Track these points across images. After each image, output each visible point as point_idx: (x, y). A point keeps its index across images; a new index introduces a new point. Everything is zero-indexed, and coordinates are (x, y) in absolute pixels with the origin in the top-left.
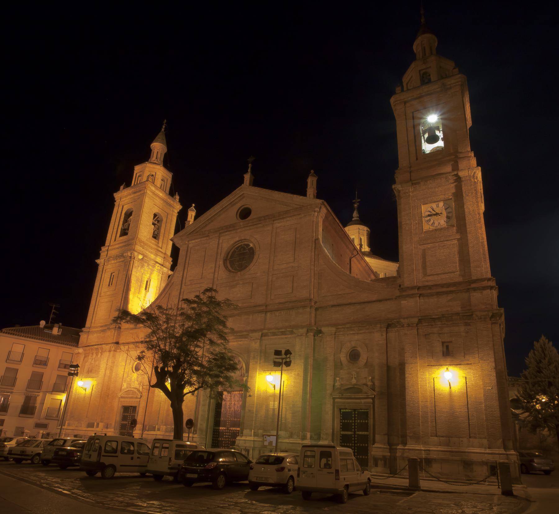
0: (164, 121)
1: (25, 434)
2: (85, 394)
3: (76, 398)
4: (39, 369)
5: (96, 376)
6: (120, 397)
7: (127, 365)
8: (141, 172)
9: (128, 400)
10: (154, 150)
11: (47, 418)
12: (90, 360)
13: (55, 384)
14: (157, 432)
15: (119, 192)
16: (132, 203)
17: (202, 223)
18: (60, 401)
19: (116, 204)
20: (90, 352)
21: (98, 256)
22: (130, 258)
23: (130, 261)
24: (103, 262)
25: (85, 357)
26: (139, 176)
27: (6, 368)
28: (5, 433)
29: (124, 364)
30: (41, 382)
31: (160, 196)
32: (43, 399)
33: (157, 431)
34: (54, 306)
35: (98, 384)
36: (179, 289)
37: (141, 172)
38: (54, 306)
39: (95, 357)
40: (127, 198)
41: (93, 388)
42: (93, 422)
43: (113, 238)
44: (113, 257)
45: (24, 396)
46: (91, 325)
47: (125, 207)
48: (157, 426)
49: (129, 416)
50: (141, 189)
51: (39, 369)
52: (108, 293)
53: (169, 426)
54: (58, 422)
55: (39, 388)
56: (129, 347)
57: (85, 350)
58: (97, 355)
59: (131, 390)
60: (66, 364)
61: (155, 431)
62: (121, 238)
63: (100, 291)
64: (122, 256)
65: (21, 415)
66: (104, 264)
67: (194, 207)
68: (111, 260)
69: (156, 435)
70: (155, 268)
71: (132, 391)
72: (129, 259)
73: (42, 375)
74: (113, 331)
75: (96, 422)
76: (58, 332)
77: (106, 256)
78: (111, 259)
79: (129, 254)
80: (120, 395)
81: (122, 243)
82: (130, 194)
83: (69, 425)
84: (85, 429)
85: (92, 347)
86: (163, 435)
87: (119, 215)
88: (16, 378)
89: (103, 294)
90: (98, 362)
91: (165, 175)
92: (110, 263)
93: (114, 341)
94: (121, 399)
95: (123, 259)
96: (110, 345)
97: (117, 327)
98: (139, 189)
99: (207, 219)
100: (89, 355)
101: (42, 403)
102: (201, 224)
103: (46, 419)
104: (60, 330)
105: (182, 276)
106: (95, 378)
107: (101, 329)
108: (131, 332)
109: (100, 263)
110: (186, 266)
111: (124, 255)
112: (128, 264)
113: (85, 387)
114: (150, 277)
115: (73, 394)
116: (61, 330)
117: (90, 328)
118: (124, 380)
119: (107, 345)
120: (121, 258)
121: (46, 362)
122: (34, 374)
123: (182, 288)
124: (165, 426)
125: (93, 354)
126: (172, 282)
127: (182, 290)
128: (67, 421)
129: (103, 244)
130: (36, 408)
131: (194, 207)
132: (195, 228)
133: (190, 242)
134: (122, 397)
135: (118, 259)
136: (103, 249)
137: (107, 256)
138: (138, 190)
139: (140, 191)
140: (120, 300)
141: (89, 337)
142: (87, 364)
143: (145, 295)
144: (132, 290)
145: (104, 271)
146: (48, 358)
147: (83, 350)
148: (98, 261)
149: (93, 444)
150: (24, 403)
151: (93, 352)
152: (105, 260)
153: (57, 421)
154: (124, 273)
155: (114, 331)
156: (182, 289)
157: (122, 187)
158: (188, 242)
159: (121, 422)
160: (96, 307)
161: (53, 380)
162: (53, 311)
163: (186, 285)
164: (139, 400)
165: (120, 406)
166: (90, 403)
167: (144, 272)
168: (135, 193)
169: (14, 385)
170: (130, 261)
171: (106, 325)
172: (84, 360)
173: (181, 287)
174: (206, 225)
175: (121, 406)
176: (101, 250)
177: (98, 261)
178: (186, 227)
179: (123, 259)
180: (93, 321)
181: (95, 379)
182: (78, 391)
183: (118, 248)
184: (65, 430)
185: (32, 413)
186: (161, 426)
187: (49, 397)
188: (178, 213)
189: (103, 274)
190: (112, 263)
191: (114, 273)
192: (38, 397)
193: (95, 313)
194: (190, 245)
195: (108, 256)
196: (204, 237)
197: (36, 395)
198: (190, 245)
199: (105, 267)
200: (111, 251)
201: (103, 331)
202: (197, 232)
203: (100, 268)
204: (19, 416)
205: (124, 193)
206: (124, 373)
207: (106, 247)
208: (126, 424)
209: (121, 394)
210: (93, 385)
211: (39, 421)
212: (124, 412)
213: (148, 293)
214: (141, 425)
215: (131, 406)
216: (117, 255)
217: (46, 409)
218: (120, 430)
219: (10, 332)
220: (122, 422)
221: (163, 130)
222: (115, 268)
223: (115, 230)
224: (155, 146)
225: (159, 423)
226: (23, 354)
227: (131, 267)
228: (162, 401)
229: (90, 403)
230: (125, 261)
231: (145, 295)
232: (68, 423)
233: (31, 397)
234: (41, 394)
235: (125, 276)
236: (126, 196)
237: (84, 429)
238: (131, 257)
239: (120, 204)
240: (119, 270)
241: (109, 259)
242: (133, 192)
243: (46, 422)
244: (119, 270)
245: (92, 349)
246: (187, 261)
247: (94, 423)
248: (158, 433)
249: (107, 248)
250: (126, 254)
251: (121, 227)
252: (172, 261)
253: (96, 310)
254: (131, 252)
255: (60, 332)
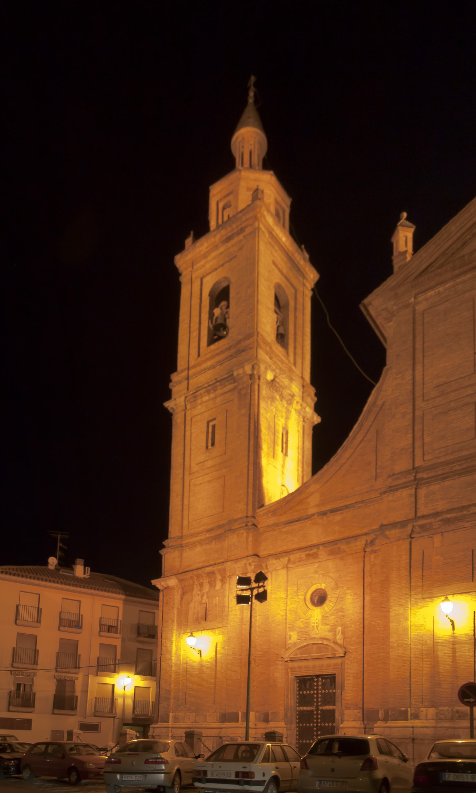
0: (249, 78)
1: (128, 736)
2: (201, 661)
3: (181, 670)
4: (70, 636)
5: (220, 625)
6: (289, 659)
7: (289, 597)
8: (227, 195)
9: (311, 663)
10: (243, 147)
11: (96, 715)
12: (197, 598)
13: (98, 658)
14: (412, 721)
15: (185, 253)
16: (223, 265)
17: (454, 238)
18: (111, 687)
19: (184, 279)
20: (194, 582)
21: (168, 395)
22: (251, 379)
23: (252, 385)
24: (183, 404)
25: (183, 594)
26: (224, 208)
27: (17, 635)
28: (78, 736)
29: (284, 596)
30: (76, 657)
31: (282, 242)
32: (86, 685)
33: (411, 719)
34: (59, 536)
35: (227, 642)
36: (411, 410)
37: (227, 195)
38: (59, 536)
39: (209, 590)
40: (209, 258)
41: (218, 649)
42: (235, 711)
43: (194, 352)
44: (206, 385)
45: (55, 681)
46: (182, 533)
47: (205, 280)
48: (409, 709)
49: (315, 696)
50: (243, 225)
51: (70, 636)
52: (210, 463)
53: (446, 708)
54: (114, 720)
55: (76, 666)
56: (289, 560)
57: (181, 581)
58: (212, 584)
59: (313, 644)
60: (110, 625)
61: (407, 720)
62: (213, 347)
63: (187, 463)
64: (230, 378)
65: (56, 711)
66: (186, 408)
67: (407, 219)
68: (201, 394)
69: (413, 727)
70: (292, 407)
71: (315, 646)
72: (250, 382)
73: (76, 644)
74: (243, 533)
75: (241, 711)
76: (84, 574)
77: (186, 390)
78: (202, 391)
79: (248, 369)
80: (287, 656)
81: (222, 352)
82: (216, 247)
83: (176, 719)
84: (218, 725)
85: (200, 572)
86: (435, 727)
87: (196, 301)
88: (36, 652)
89: (195, 468)
90: (217, 598)
91: (279, 199)
92: (199, 401)
93: (251, 553)
94: (290, 664)
95: (230, 387)
96: (244, 561)
97: (250, 524)
98: (238, 227)
99: (468, 226)
100: (193, 589)
101: (85, 691)
102: (450, 242)
103: (95, 716)
104: (88, 569)
105: (411, 382)
106: (218, 629)
107: (208, 535)
108: (284, 530)
109: (175, 408)
110: (419, 356)
111: (235, 374)
112: (249, 391)
113: (199, 648)
114: (286, 424)
115: (173, 664)
116: (89, 568)
117: (181, 537)
118: (288, 626)
119: (235, 563)
120: (227, 384)
121: (78, 622)
122: (63, 643)
123: (417, 407)
124: (433, 709)
125: (201, 585)
126: (379, 403)
127: (418, 413)
128: (171, 714)
129: (173, 367)
130: (77, 700)
131: (407, 219)
132: (434, 258)
133: (421, 298)
134: (292, 660)
135: (219, 387)
136: (175, 377)
137: (188, 389)
138: (235, 231)
139: (242, 230)
140: (245, 471)
141: (184, 555)
142: (192, 605)
143: (284, 460)
144: (265, 447)
145: (188, 422)
146: (80, 617)
147: (176, 581)
148: (168, 405)
149: (192, 750)
150: (57, 691)
151: (201, 581)
152: (187, 398)
153: (113, 719)
154: (243, 411)
155: (245, 534)
156: (417, 411)
157: (189, 241)
158: (415, 298)
159: (298, 708)
160: (186, 495)
161: (95, 653)
162: (59, 544)
163: (426, 399)
164: (339, 661)
165: (291, 676)
166: (216, 678)
167: (277, 412)
168: (228, 239)
169: (35, 662)
170: (251, 384)
171: (219, 527)
172: (182, 599)
173: (414, 406)
174: (465, 244)
175: (293, 677)
176: (170, 381)
177: (168, 405)
178: (396, 268)
179: (230, 387)
180: (185, 523)
181: (217, 631)
182: (181, 657)
183: (213, 367)
184: (170, 729)
185: (73, 707)
186: (422, 709)
187: (93, 680)
188: (313, 290)
189: (187, 429)
190: (206, 401)
191: (214, 419)
192: (76, 681)
193: (185, 507)
194: (417, 308)
195: (190, 390)
196: (465, 272)
197: (72, 677)
198: (420, 308)
199: (188, 413)
200: (197, 378)
201: (218, 538)
202: (442, 266)
203: (177, 419)
204: (54, 714)
205: (201, 248)
206: (286, 613)
207: (182, 371)
208: (312, 711)
209: (290, 653)
210: (217, 644)
211: (84, 720)
212: (300, 688)
213: (287, 459)
214: (356, 711)
215: (317, 676)
216: (216, 379)
217: (92, 700)
218: (298, 723)
219: (11, 571)
220: (301, 708)
221: (251, 101)
222: (214, 410)
223: (195, 334)
224: (243, 138)
225: (413, 702)
226: (39, 611)
227: (256, 397)
228: (412, 656)
229: (216, 678)
230: (240, 387)
231: (284, 460)
232: (172, 717)
233: (65, 680)
234: (80, 676)
235: (248, 419)
236: (205, 256)
237: (214, 726)
238: (251, 376)
239: (194, 276)
240: (227, 411)
241: (196, 394)
242: (224, 238)
243: (95, 721)
244: (227, 411)
245: (198, 576)
246: (419, 346)
247: (237, 714)
248: (417, 723)
249: (185, 374)
250: (241, 371)
251: (207, 325)
252: (316, 395)
253: (186, 502)
254: (253, 363)
255: (88, 573)
